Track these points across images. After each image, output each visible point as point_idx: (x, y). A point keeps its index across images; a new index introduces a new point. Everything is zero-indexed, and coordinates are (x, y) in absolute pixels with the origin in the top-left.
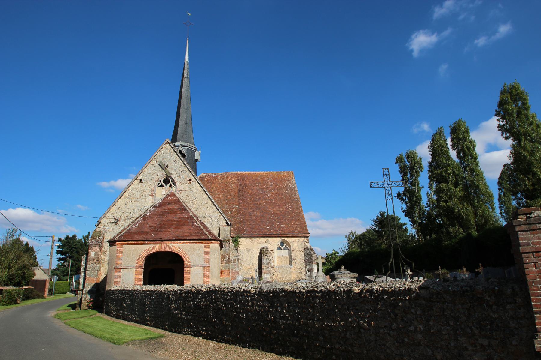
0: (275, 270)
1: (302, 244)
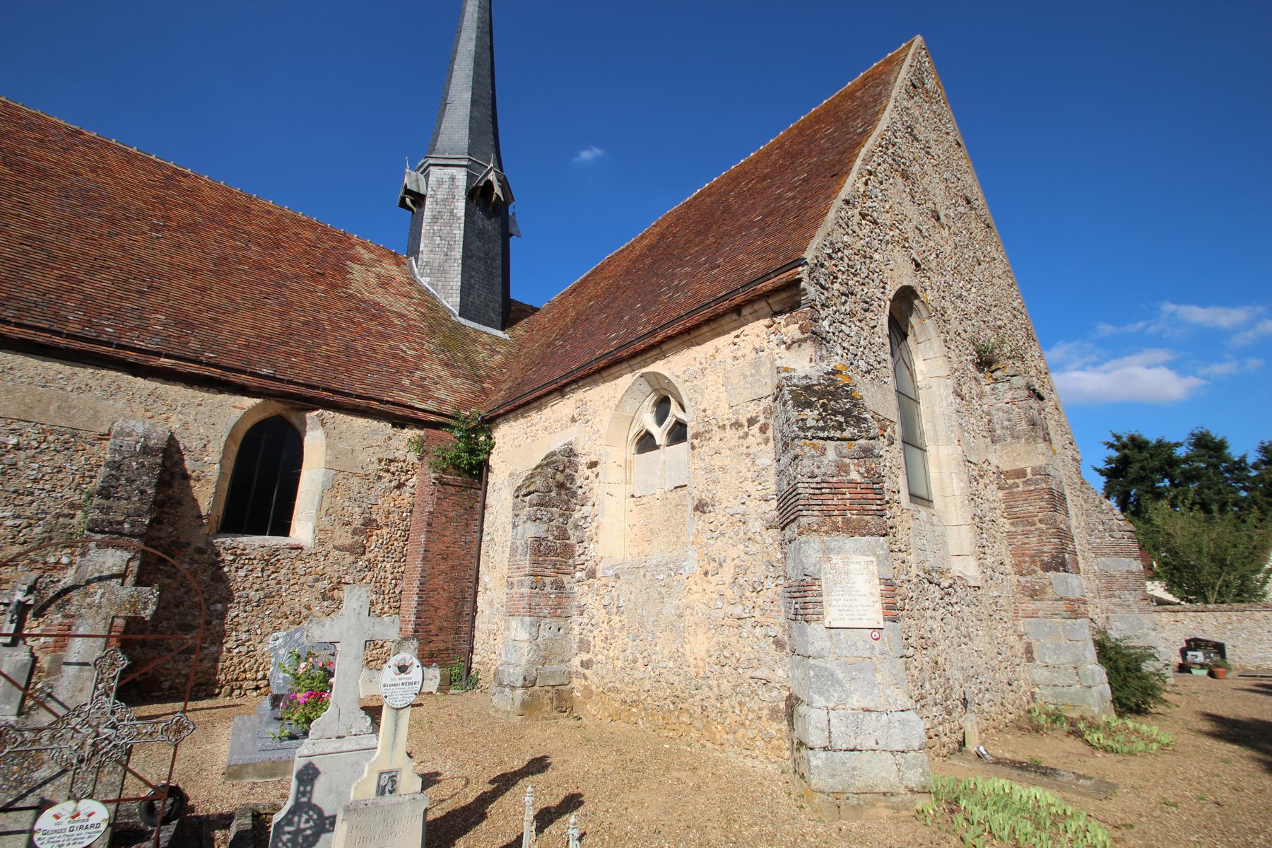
1: (756, 365)
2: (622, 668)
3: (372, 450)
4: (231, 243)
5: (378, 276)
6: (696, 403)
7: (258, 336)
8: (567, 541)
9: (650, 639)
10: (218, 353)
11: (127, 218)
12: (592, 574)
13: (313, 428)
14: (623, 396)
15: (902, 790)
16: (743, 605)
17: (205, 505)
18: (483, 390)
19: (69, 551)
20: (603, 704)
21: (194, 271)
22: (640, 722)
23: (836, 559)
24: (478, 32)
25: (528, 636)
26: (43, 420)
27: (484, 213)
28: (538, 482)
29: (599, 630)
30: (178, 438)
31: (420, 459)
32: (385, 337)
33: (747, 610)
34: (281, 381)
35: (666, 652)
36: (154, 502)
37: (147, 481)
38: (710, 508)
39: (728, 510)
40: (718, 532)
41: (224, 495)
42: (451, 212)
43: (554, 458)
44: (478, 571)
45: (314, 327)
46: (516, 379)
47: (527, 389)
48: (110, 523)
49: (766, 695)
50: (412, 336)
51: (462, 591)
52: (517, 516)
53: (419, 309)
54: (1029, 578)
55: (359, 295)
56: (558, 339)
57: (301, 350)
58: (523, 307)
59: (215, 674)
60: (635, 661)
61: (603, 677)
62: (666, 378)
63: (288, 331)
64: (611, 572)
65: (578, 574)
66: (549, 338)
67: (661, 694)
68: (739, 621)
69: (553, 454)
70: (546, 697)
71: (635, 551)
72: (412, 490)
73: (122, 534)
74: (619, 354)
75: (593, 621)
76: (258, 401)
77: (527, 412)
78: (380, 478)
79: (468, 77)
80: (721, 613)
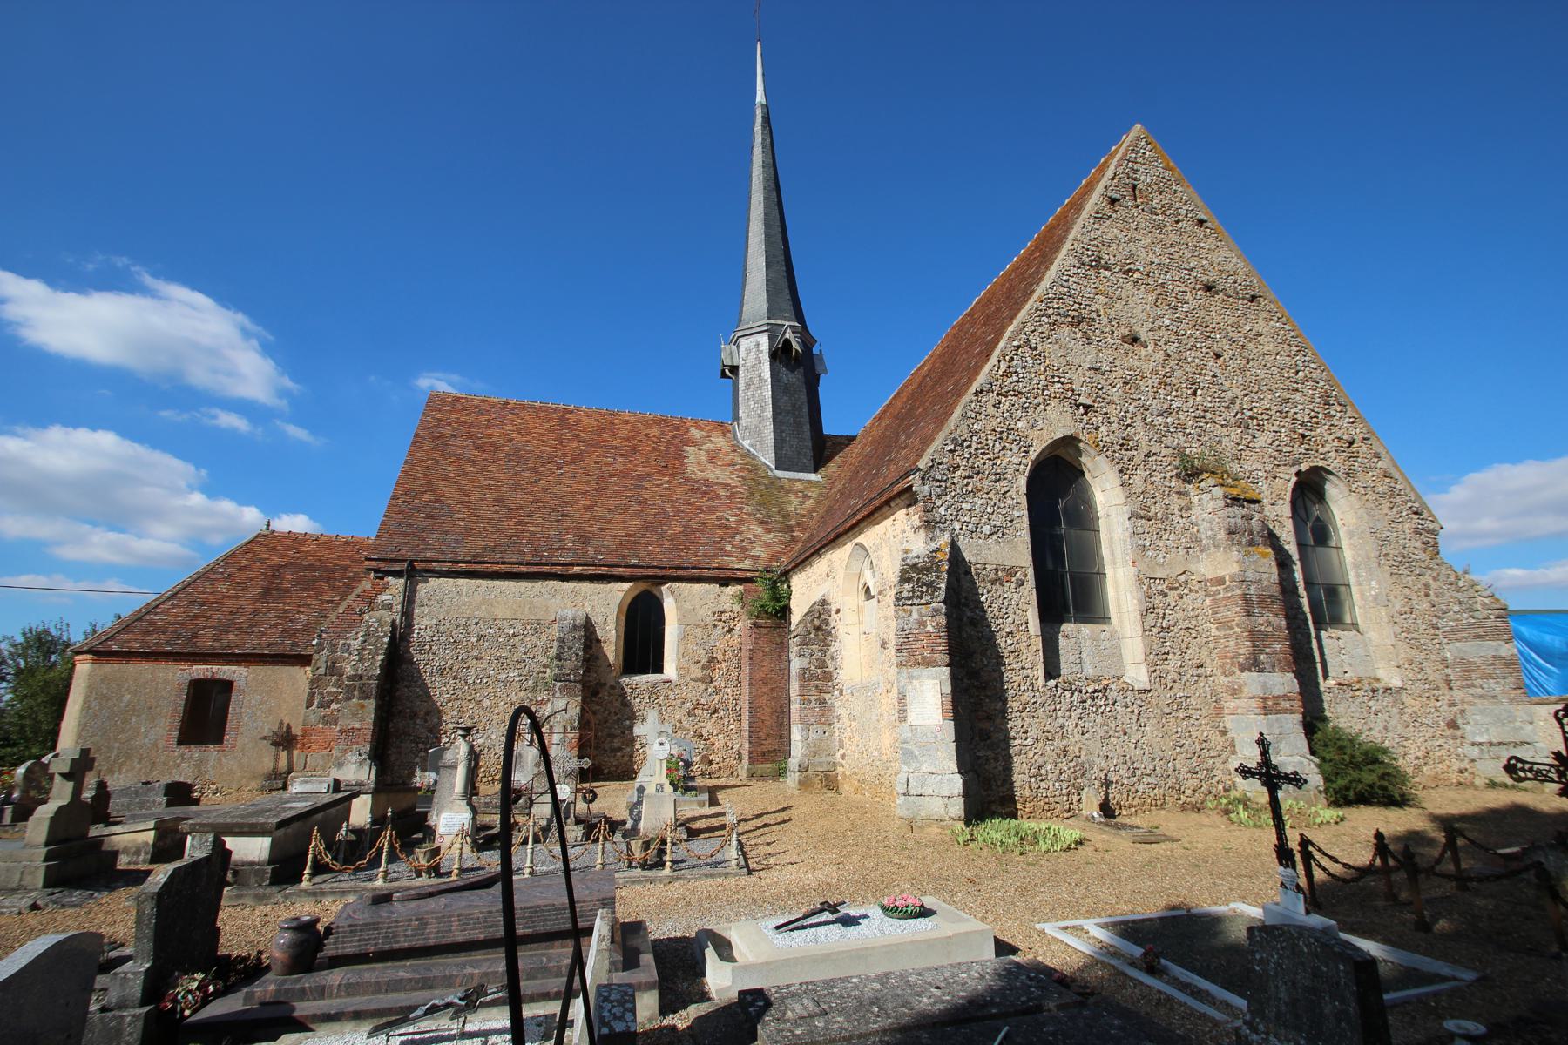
4: (605, 460)
5: (708, 452)
10: (605, 554)
11: (543, 465)
13: (667, 597)
15: (947, 818)
17: (611, 658)
23: (915, 683)
24: (765, 193)
27: (787, 369)
32: (712, 510)
34: (642, 567)
36: (584, 661)
37: (578, 647)
42: (760, 376)
45: (662, 516)
50: (734, 503)
53: (741, 474)
54: (1230, 679)
58: (839, 439)
59: (632, 765)
63: (646, 526)
73: (570, 681)
76: (631, 584)
78: (715, 626)
79: (761, 242)
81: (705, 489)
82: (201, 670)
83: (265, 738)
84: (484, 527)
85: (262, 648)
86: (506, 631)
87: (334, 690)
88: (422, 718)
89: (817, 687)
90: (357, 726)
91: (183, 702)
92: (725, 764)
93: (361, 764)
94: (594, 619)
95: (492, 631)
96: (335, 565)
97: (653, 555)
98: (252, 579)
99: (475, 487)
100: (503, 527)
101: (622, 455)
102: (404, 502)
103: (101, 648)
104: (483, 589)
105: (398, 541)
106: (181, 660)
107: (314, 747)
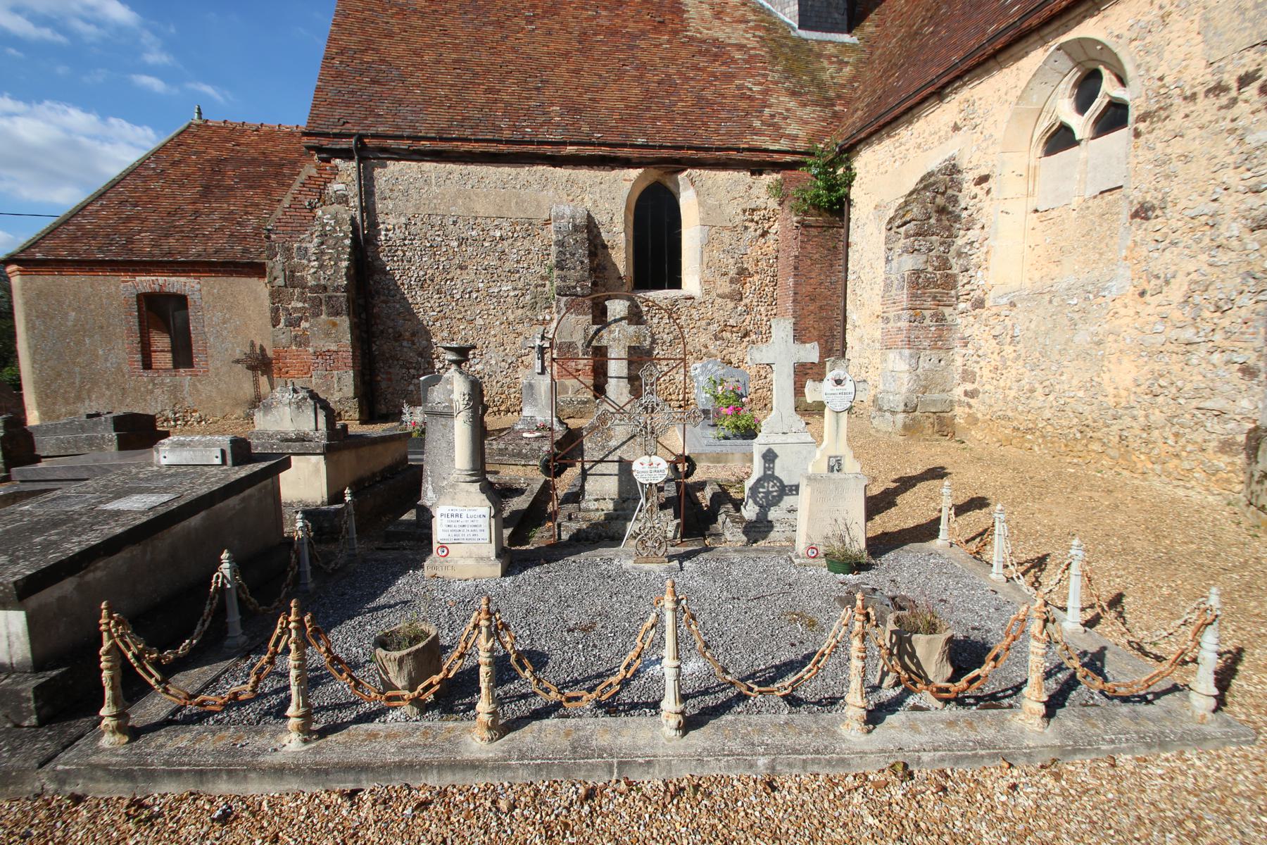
0: (992, 322)
2: (1015, 398)
3: (736, 202)
6: (1148, 70)
7: (627, 107)
8: (949, 271)
9: (1053, 368)
11: (509, 18)
12: (979, 304)
13: (685, 189)
14: (1028, 83)
16: (1197, 328)
18: (836, 115)
19: (547, 311)
20: (991, 430)
21: (566, 55)
22: (1036, 448)
25: (907, 367)
26: (510, 216)
28: (915, 210)
29: (988, 360)
30: (593, 215)
31: (780, 205)
32: (729, 77)
33: (1202, 334)
34: (653, 147)
35: (1075, 382)
36: (591, 269)
37: (582, 252)
38: (1158, 212)
39: (1187, 212)
40: (1168, 241)
41: (631, 261)
43: (932, 179)
44: (845, 310)
46: (874, 91)
47: (891, 101)
48: (569, 288)
49: (1217, 427)
50: (755, 68)
51: (831, 329)
52: (890, 249)
53: (757, 33)
55: (698, 35)
56: (926, 26)
57: (662, 113)
60: (1032, 391)
61: (991, 406)
62: (1098, 42)
63: (648, 95)
64: (1005, 300)
65: (962, 306)
66: (911, 27)
67: (1065, 423)
68: (1188, 347)
69: (930, 174)
70: (927, 422)
71: (1037, 276)
72: (776, 237)
73: (577, 296)
74: (1026, 24)
75: (980, 353)
76: (640, 171)
77: (894, 129)
78: (746, 228)
80: (1161, 338)
81: (716, 50)
82: (147, 282)
83: (238, 361)
84: (446, 96)
85: (209, 255)
86: (492, 233)
87: (300, 305)
88: (408, 340)
89: (934, 298)
90: (333, 347)
91: (136, 320)
92: (758, 395)
93: (299, 407)
94: (597, 218)
95: (474, 233)
96: (282, 159)
97: (664, 132)
98: (188, 176)
99: (428, 46)
100: (470, 95)
101: (605, 8)
102: (341, 62)
103: (23, 256)
104: (456, 176)
105: (339, 112)
106: (119, 271)
107: (292, 372)
